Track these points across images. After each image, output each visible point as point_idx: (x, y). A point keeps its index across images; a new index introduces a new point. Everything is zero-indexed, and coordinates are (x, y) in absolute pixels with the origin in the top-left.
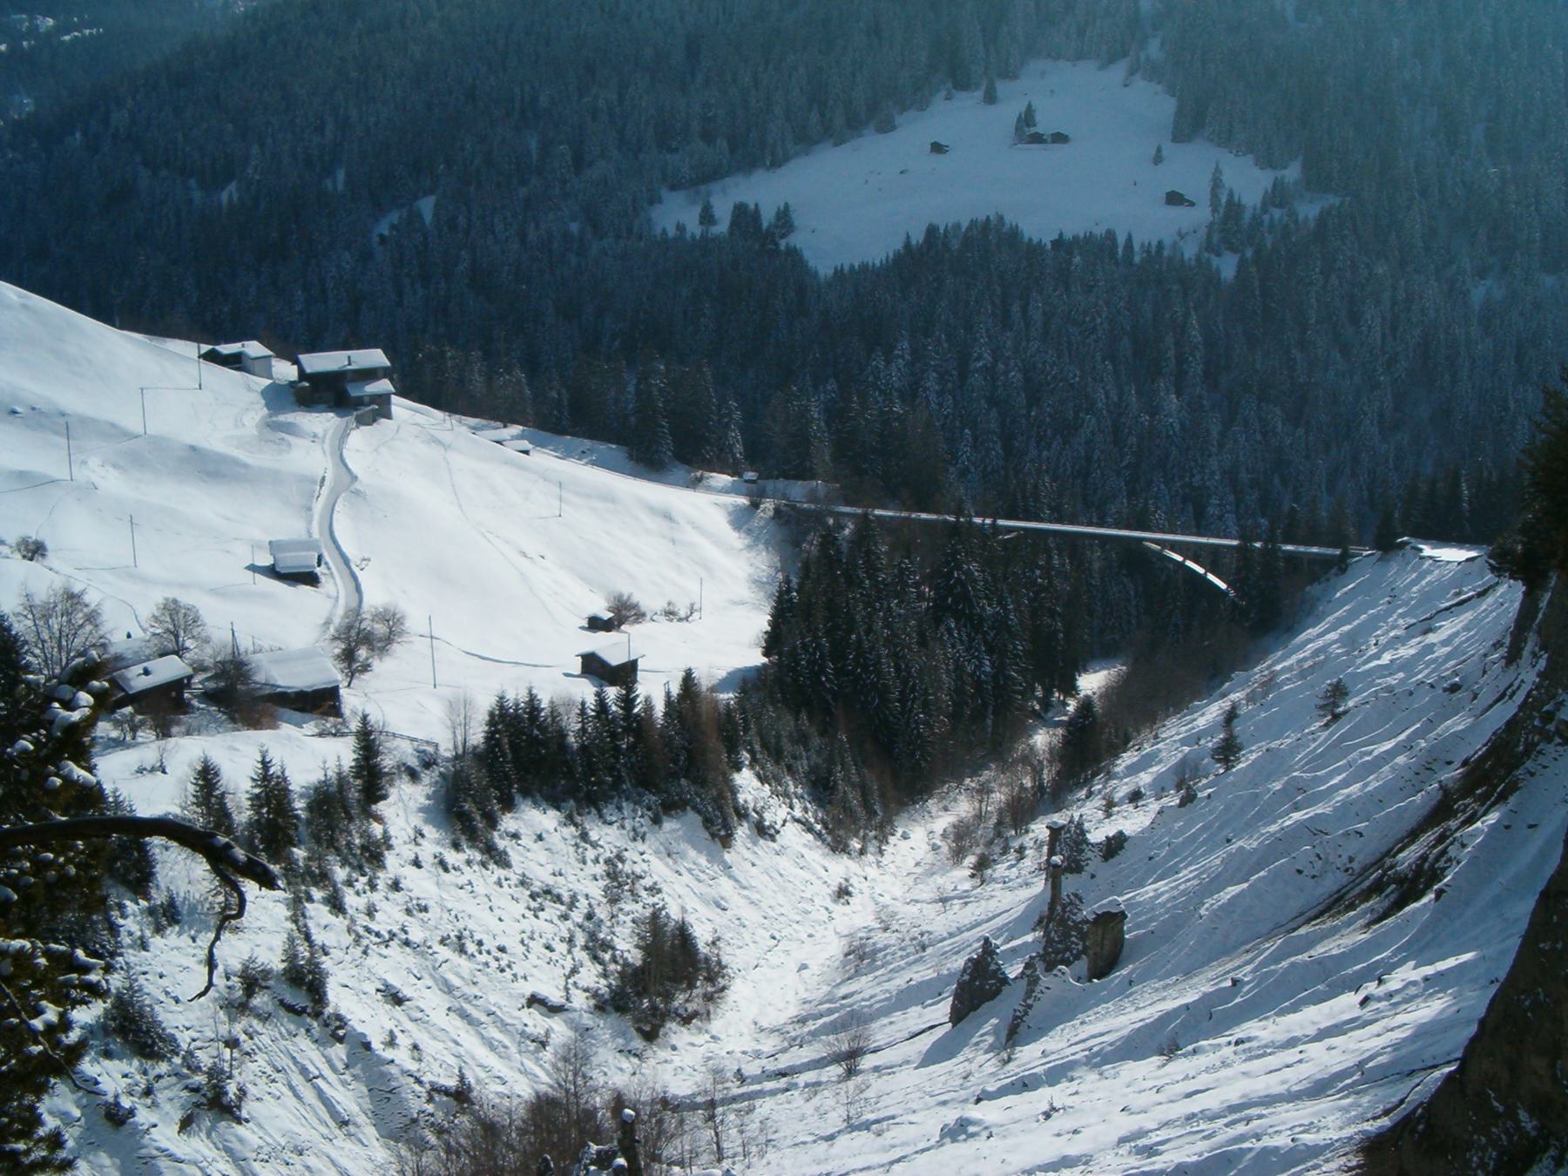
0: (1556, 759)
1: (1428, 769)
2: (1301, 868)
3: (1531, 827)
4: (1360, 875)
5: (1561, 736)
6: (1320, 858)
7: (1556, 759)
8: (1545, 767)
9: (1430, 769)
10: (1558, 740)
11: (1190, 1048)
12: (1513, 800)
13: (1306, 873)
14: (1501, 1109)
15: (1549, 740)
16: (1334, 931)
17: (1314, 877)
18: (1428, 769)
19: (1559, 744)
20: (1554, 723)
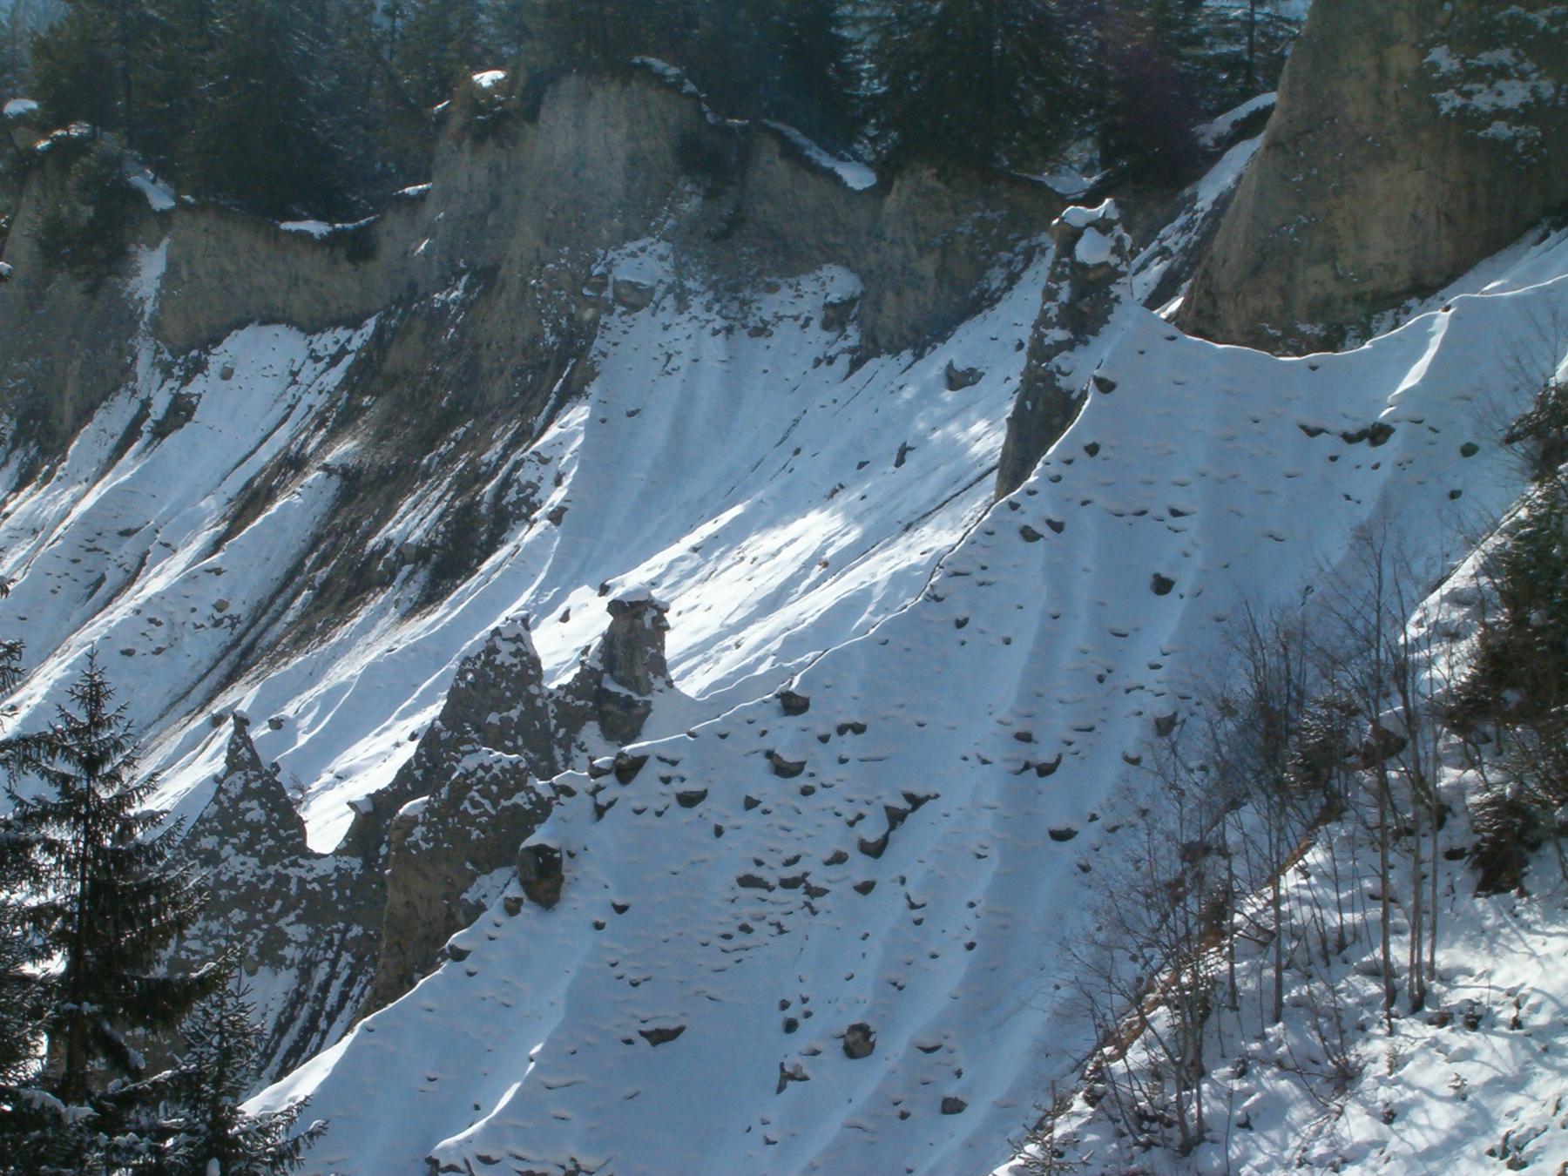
0: (625, 332)
1: (89, 550)
2: (129, 647)
3: (631, 414)
4: (254, 621)
5: (623, 304)
6: (159, 624)
7: (625, 332)
8: (615, 344)
9: (95, 549)
10: (620, 309)
11: (327, 777)
12: (594, 389)
13: (139, 650)
14: (1279, 333)
15: (611, 311)
16: (345, 647)
17: (159, 651)
18: (89, 550)
19: (624, 313)
20: (610, 289)
